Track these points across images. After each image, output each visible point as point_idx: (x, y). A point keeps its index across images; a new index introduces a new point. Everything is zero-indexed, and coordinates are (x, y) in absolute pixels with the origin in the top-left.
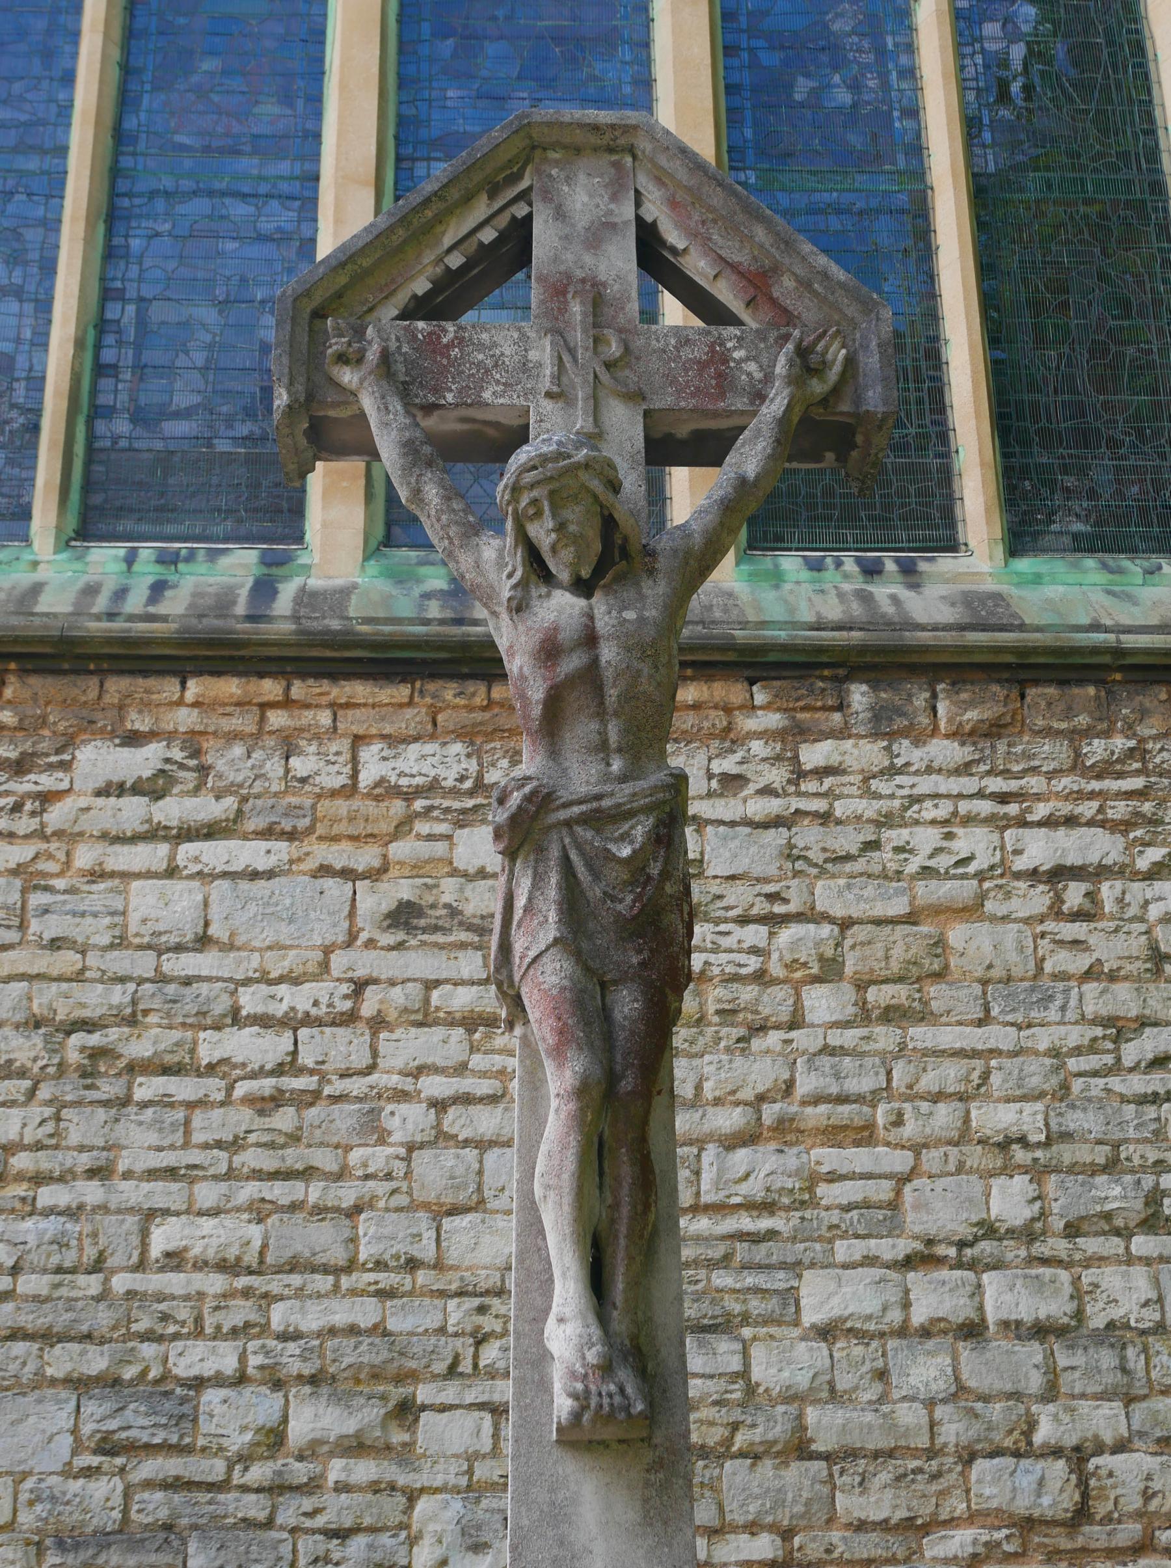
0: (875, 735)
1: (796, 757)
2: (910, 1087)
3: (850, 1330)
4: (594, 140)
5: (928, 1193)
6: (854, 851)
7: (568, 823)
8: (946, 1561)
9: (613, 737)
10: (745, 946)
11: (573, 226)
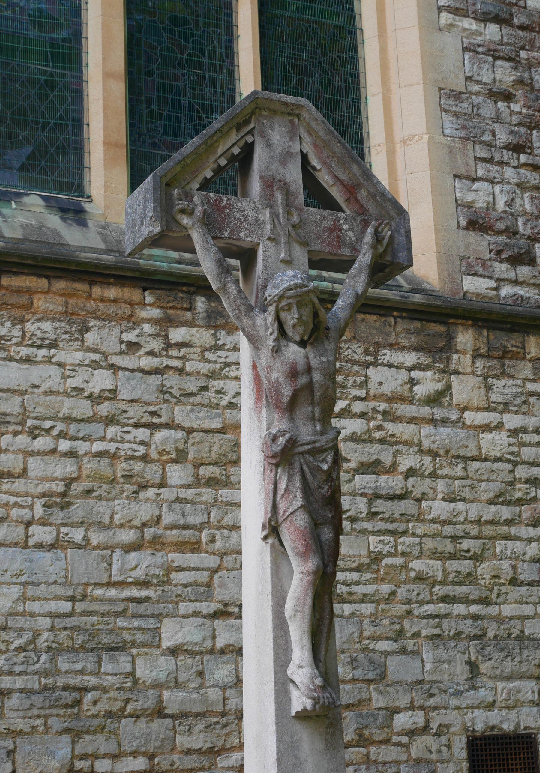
0: (208, 326)
1: (167, 335)
2: (219, 522)
3: (186, 650)
4: (283, 109)
5: (226, 579)
6: (195, 391)
7: (302, 453)
8: (229, 769)
9: (317, 414)
10: (138, 440)
11: (274, 152)
